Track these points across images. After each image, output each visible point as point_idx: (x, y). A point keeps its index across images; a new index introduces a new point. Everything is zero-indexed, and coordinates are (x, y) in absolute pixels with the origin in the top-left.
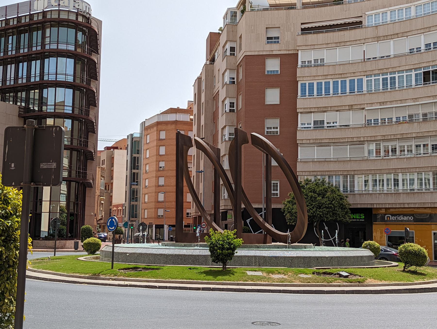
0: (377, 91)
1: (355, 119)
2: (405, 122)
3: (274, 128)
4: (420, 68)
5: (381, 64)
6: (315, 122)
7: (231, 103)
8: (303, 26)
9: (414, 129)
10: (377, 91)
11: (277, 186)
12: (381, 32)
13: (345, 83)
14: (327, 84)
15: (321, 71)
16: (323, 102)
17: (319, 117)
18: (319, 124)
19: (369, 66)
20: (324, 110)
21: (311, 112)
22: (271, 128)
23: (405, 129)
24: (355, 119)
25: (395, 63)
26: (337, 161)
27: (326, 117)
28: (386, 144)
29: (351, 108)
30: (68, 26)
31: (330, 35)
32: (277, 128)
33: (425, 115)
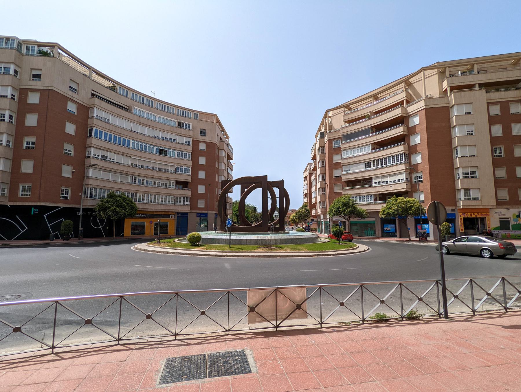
0: (137, 150)
1: (124, 160)
2: (149, 169)
3: (69, 151)
4: (159, 147)
5: (141, 137)
6: (102, 156)
7: (10, 115)
8: (93, 92)
9: (155, 174)
10: (137, 150)
11: (68, 192)
12: (142, 120)
13: (119, 139)
14: (110, 135)
15: (108, 126)
16: (107, 146)
17: (105, 153)
18: (104, 158)
19: (134, 135)
20: (108, 150)
21: (100, 149)
22: (66, 150)
23: (150, 173)
24: (124, 160)
25: (148, 139)
26: (113, 182)
27: (109, 155)
28: (140, 178)
29: (123, 154)
30: (409, 180)
31: (115, 108)
32: (71, 151)
33: (159, 169)
